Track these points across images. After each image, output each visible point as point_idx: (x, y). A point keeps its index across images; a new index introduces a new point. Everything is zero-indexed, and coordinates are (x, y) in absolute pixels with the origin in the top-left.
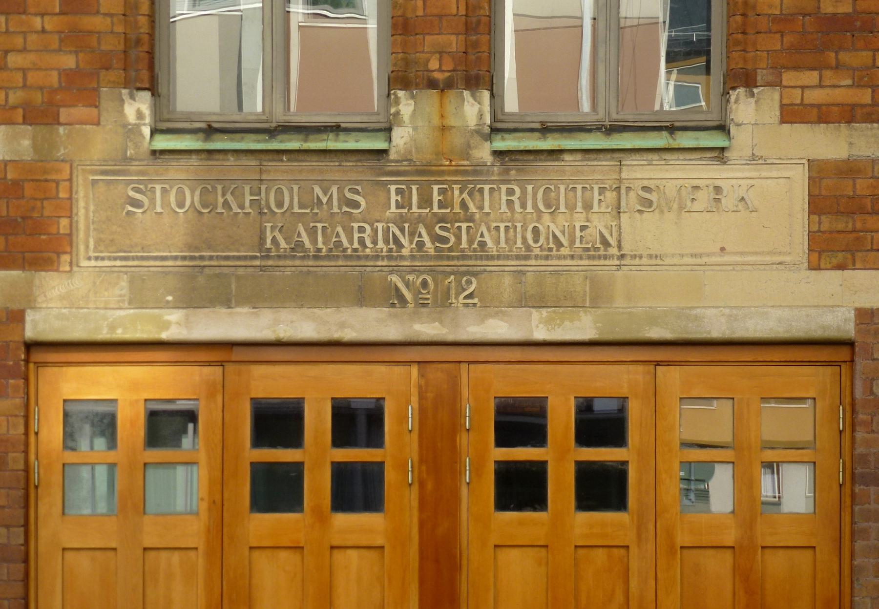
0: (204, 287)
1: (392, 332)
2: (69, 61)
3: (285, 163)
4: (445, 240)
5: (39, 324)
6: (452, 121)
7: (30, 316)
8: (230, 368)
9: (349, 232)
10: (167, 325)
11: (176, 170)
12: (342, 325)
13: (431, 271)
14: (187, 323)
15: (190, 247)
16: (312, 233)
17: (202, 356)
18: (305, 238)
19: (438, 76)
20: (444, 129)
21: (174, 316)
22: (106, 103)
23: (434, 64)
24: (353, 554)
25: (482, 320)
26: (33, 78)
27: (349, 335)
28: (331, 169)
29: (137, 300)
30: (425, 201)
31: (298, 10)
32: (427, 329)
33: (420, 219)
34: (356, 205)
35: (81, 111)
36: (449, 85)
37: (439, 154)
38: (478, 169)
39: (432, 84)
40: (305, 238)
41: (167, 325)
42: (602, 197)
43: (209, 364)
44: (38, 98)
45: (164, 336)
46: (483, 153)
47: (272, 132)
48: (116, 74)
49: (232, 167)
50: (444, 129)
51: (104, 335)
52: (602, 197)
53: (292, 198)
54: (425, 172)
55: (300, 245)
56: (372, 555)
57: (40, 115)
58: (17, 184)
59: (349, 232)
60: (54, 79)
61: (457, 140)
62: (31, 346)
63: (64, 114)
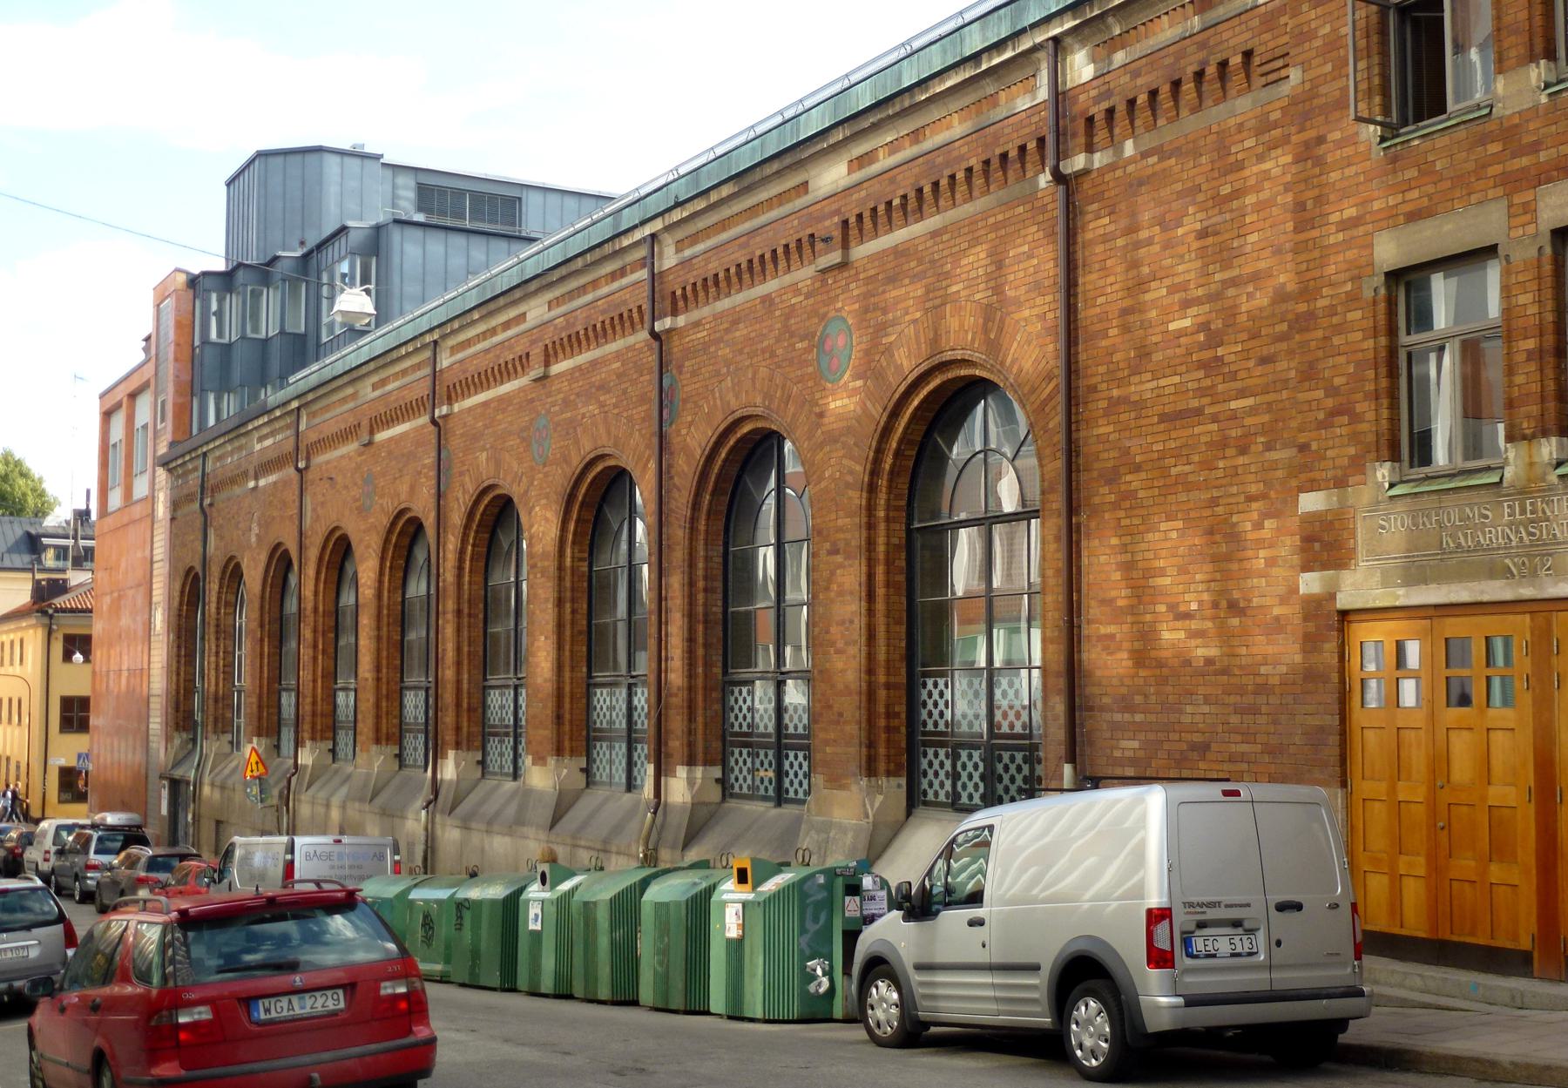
0: (1415, 574)
1: (1508, 595)
2: (1352, 451)
3: (1452, 496)
4: (1533, 534)
5: (1344, 601)
6: (1536, 459)
7: (1339, 596)
8: (1436, 621)
9: (1484, 534)
10: (1398, 597)
11: (1400, 506)
12: (1482, 592)
13: (1528, 555)
14: (1407, 595)
15: (1409, 551)
16: (1466, 536)
17: (1413, 613)
18: (1462, 540)
19: (1527, 432)
20: (1531, 464)
21: (1401, 591)
22: (1369, 472)
23: (1525, 425)
24: (1500, 733)
25: (1556, 584)
26: (1338, 462)
27: (1486, 598)
28: (1474, 496)
29: (1385, 583)
30: (1523, 512)
31: (2, 670)
32: (1527, 592)
33: (1521, 523)
34: (1486, 517)
35: (1358, 478)
36: (1534, 436)
37: (1529, 480)
38: (1551, 488)
39: (1524, 438)
40: (1462, 540)
41: (1398, 597)
42: (289, 857)
43: (1425, 618)
44: (1339, 473)
45: (1397, 604)
46: (1553, 477)
47: (1452, 476)
48: (1373, 455)
49: (1426, 502)
50: (1531, 464)
51: (1370, 605)
52: (289, 857)
53: (1455, 515)
54: (1523, 492)
55: (1459, 545)
56: (1508, 734)
57: (1340, 483)
58: (1331, 522)
59: (1484, 534)
60: (1346, 461)
61: (1538, 470)
62: (1344, 614)
63: (1351, 480)
